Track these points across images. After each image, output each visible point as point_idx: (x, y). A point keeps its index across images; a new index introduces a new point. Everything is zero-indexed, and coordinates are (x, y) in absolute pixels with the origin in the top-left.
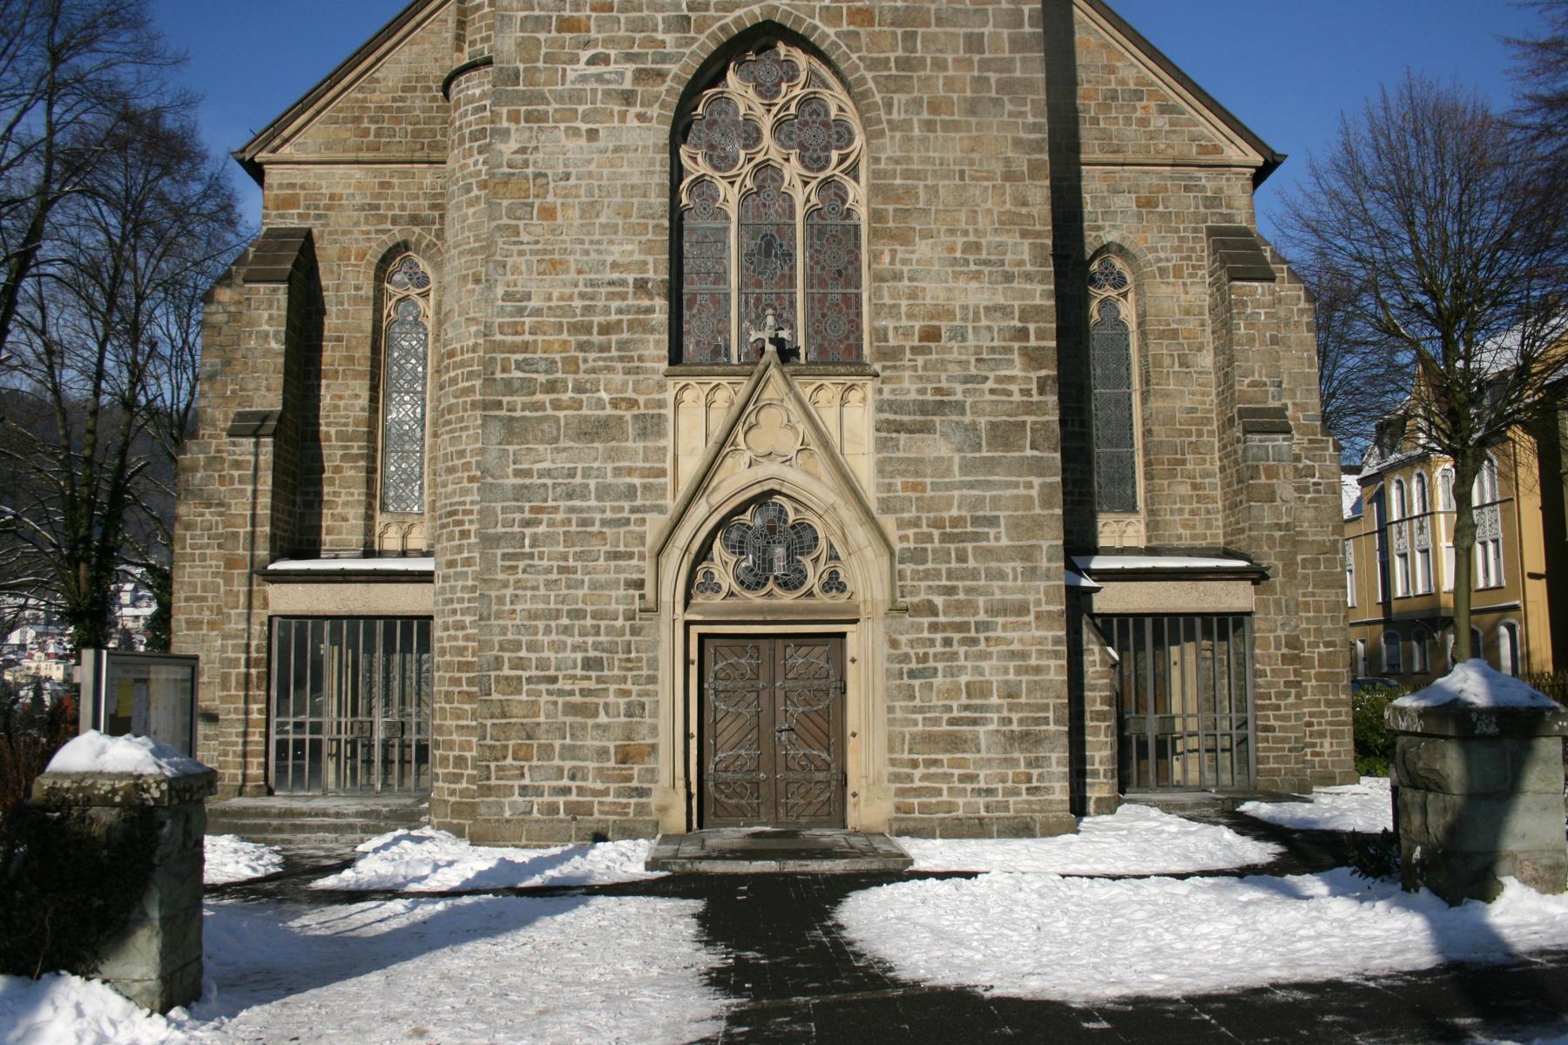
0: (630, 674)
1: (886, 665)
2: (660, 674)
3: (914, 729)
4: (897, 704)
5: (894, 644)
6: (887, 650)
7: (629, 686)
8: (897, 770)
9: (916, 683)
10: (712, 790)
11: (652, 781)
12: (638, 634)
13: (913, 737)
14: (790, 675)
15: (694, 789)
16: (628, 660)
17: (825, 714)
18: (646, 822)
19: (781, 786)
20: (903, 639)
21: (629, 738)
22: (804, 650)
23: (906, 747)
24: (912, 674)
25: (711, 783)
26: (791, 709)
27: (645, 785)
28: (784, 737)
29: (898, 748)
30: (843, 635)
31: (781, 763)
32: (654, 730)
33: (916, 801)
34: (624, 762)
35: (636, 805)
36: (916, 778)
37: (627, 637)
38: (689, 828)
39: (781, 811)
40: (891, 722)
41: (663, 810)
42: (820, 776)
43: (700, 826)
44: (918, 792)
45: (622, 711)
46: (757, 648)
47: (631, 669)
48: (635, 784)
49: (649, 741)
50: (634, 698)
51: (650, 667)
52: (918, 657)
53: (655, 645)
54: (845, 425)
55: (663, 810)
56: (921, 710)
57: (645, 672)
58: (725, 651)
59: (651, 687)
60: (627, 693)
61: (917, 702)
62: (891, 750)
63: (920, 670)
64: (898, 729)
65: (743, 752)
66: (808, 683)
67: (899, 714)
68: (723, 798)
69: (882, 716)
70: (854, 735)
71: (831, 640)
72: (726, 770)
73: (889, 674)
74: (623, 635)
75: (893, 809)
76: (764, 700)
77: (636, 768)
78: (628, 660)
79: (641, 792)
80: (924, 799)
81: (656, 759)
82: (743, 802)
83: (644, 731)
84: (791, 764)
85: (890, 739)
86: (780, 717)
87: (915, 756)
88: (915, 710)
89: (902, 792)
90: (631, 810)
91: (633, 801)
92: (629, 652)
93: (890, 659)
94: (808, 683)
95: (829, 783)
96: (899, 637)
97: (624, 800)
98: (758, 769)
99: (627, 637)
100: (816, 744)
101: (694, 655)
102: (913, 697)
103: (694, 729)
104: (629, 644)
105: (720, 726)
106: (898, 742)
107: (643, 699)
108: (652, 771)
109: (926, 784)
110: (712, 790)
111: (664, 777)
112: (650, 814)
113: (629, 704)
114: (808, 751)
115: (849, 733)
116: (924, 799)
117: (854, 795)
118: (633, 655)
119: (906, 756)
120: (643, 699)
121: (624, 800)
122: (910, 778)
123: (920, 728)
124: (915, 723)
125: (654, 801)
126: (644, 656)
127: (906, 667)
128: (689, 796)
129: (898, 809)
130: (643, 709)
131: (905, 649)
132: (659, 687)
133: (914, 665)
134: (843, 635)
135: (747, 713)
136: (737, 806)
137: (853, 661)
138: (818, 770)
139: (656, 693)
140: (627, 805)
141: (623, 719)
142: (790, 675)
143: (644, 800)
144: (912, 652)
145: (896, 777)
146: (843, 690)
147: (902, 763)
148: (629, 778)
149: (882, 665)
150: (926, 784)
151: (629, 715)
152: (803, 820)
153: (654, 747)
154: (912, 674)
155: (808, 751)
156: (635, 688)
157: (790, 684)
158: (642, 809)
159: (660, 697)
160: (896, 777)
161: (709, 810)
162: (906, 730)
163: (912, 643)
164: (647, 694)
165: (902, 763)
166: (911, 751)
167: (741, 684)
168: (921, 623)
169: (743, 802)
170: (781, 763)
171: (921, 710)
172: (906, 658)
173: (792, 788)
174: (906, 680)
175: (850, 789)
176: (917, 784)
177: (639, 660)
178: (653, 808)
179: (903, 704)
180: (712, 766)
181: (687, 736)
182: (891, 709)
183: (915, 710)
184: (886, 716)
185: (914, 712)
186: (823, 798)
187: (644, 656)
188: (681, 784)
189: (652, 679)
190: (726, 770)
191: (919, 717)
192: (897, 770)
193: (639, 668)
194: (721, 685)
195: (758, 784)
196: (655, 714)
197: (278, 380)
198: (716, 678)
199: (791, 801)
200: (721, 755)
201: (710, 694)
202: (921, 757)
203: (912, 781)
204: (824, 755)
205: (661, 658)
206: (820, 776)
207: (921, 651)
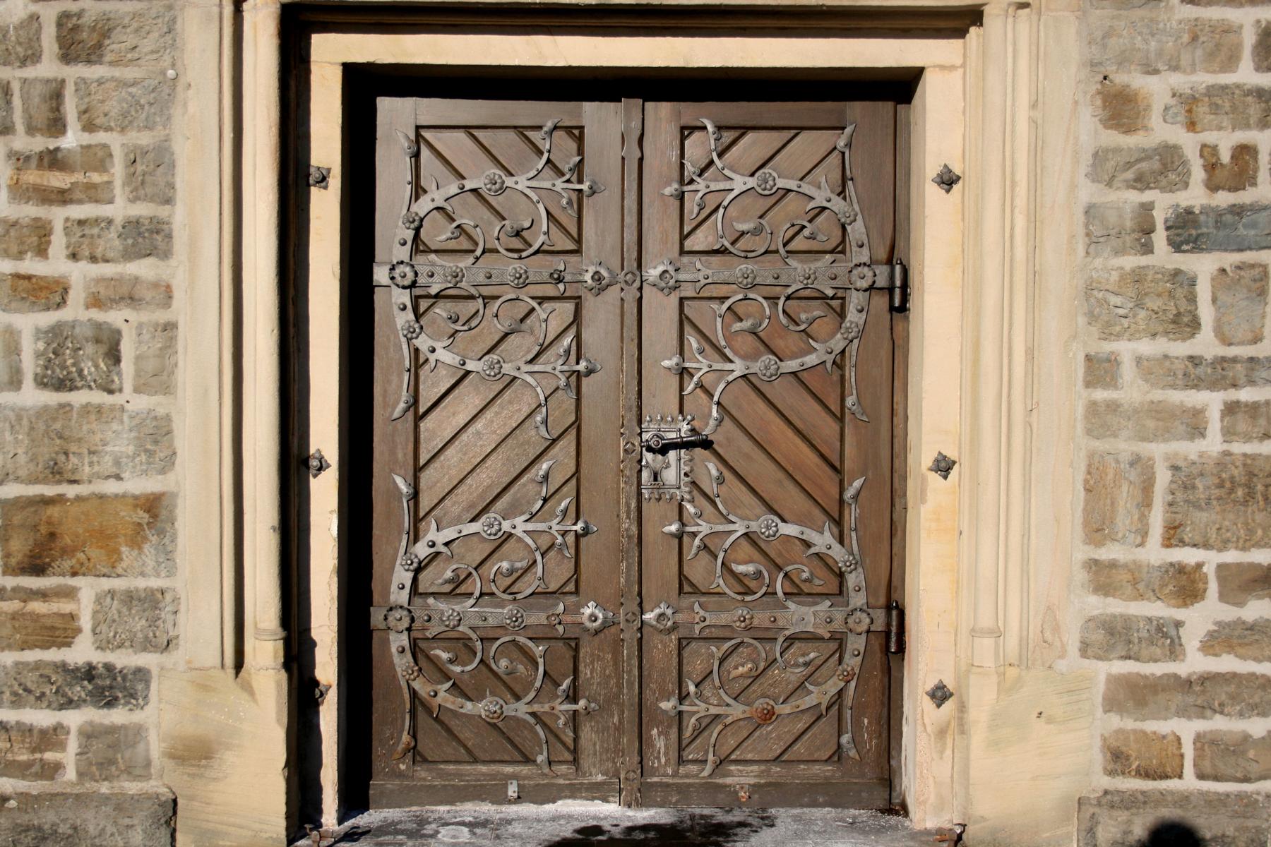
0: (58, 215)
1: (1088, 192)
2: (179, 217)
3: (1190, 449)
4: (1127, 349)
5: (1120, 108)
6: (1089, 130)
7: (56, 265)
8: (1116, 606)
9: (1203, 266)
10: (402, 663)
11: (148, 645)
12: (93, 54)
13: (1185, 478)
14: (699, 241)
15: (326, 668)
16: (52, 160)
17: (828, 386)
18: (121, 805)
19: (662, 650)
20: (1157, 89)
21: (56, 473)
22: (753, 146)
23: (1157, 519)
24: (1188, 231)
25: (399, 641)
26: (701, 365)
27: (123, 659)
28: (673, 468)
29: (1124, 520)
30: (900, 87)
31: (661, 565)
32: (156, 440)
33: (1187, 729)
34: (37, 567)
35: (89, 734)
36: (1192, 638)
37: (48, 67)
38: (302, 810)
39: (660, 742)
40: (1100, 419)
41: (196, 754)
42: (804, 616)
43: (355, 797)
44: (1200, 693)
45: (29, 365)
46: (577, 134)
47: (63, 197)
48: (82, 652)
49: (138, 484)
50: (75, 311)
51: (138, 187)
52: (1212, 167)
53: (162, 96)
54: (780, 145)
55: (196, 754)
56: (1218, 373)
57: (120, 209)
58: (454, 145)
59: (144, 269)
60: (49, 293)
61: (1205, 344)
62: (1097, 530)
63: (1218, 216)
64: (1125, 446)
65: (519, 525)
66: (764, 271)
67: (1132, 390)
68: (444, 697)
69: (1066, 396)
70: (944, 467)
71: (856, 110)
72: (456, 589)
73: (1098, 230)
74: (33, 57)
75: (1097, 758)
76: (602, 319)
77: (88, 589)
78: (52, 160)
79: (107, 686)
80: (1218, 724)
81: (167, 556)
82: (520, 709)
83: (119, 442)
84: (698, 570)
85: (1096, 486)
86: (661, 396)
87: (1188, 556)
88: (1199, 373)
89: (1134, 695)
90: (69, 757)
91: (74, 719)
92: (57, 125)
93: (1103, 167)
94: (764, 271)
95: (839, 640)
96: (1136, 81)
97: (41, 718)
98: (576, 586)
99: (48, 67)
100: (791, 498)
101: (326, 145)
102: (1186, 324)
103: (324, 434)
104: (56, 96)
105: (436, 428)
106: (1125, 498)
107: (114, 317)
108: (152, 602)
109: (1227, 663)
110: (402, 663)
111: (200, 626)
112: (141, 770)
113: (57, 338)
114: (762, 524)
115: (922, 456)
116: (1218, 724)
117: (940, 695)
118: (71, 140)
119: (1155, 554)
120: (114, 317)
121: (41, 718)
122: (1166, 638)
123: (1213, 444)
124: (1195, 426)
125: (158, 719)
126: (115, 142)
127: (1163, 204)
128: (303, 696)
129: (1117, 759)
130: (114, 356)
131: (1162, 130)
132: (175, 270)
133: (1195, 196)
134: (900, 87)
135: (540, 382)
136: (497, 727)
137: (948, 181)
138: (796, 592)
139: (166, 295)
140: (51, 738)
141: (32, 397)
142: (699, 241)
143: (118, 716)
144: (1189, 143)
145: (1113, 637)
146: (898, 299)
147: (1135, 581)
148: (60, 632)
149: (1071, 189)
150: (1227, 663)
151: (58, 379)
152: (741, 778)
153: (155, 509)
154: (1188, 231)
155: (762, 524)
156: (79, 274)
157: (702, 270)
158: (109, 752)
159: (179, 310)
160: (1113, 637)
161: (392, 736)
162: (1158, 451)
163: (1190, 109)
164: (129, 296)
165: (1135, 581)
166: (1173, 536)
167: (509, 267)
168: (1229, 30)
169: (520, 709)
170: (661, 565)
171: (1218, 373)
172: (1164, 167)
173: (700, 659)
174: (1163, 256)
175: (925, 665)
176: (1194, 663)
177: (98, 159)
178: (155, 747)
179: (1147, 347)
180: (403, 576)
181: (294, 465)
182: (1100, 370)
183: (1199, 373)
184: (1083, 396)
185: (1195, 384)
186: (817, 696)
187: (115, 142)
188: (265, 651)
189: (148, 238)
190: (456, 589)
191: (1212, 401)
192: (1116, 606)
193: (95, 194)
194: (437, 273)
195: (573, 645)
196: (159, 379)
197: (314, 56)
198: (418, 245)
199: (697, 709)
200: (434, 534)
201: (392, 307)
202: (1211, 560)
203: (1175, 650)
204: (823, 540)
205: (182, 150)
206: (804, 616)
207: (1226, 142)
